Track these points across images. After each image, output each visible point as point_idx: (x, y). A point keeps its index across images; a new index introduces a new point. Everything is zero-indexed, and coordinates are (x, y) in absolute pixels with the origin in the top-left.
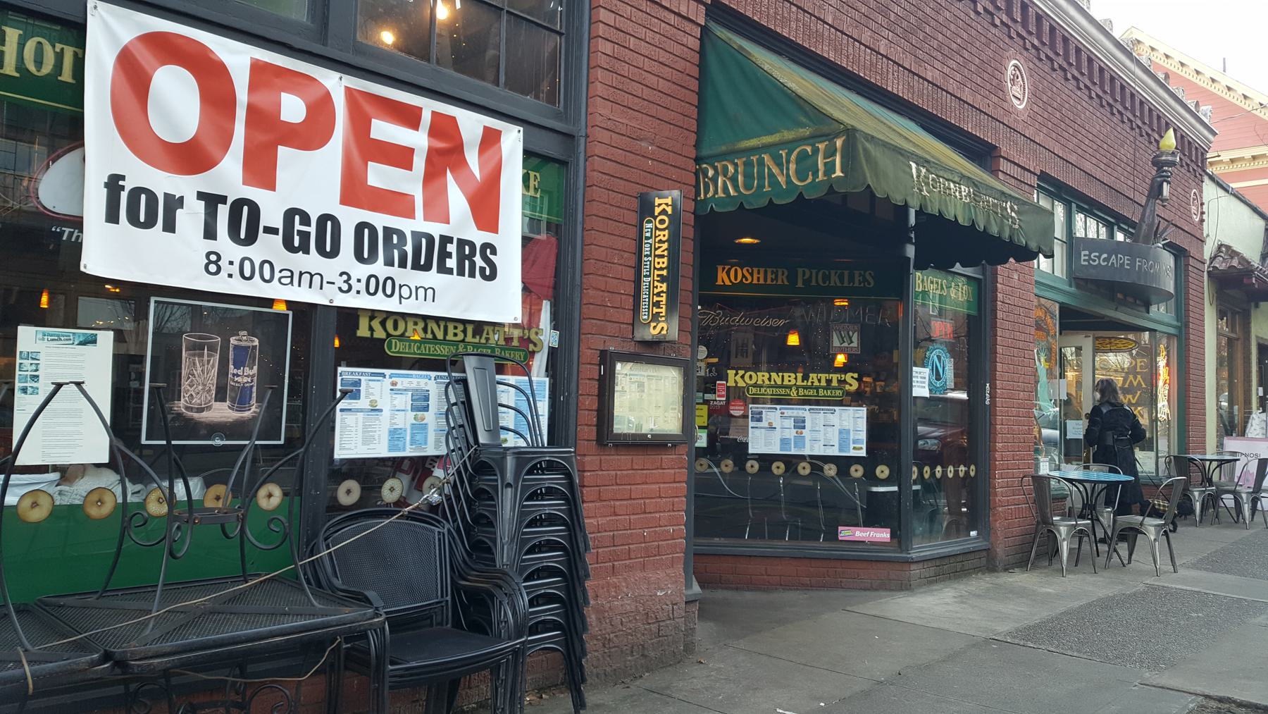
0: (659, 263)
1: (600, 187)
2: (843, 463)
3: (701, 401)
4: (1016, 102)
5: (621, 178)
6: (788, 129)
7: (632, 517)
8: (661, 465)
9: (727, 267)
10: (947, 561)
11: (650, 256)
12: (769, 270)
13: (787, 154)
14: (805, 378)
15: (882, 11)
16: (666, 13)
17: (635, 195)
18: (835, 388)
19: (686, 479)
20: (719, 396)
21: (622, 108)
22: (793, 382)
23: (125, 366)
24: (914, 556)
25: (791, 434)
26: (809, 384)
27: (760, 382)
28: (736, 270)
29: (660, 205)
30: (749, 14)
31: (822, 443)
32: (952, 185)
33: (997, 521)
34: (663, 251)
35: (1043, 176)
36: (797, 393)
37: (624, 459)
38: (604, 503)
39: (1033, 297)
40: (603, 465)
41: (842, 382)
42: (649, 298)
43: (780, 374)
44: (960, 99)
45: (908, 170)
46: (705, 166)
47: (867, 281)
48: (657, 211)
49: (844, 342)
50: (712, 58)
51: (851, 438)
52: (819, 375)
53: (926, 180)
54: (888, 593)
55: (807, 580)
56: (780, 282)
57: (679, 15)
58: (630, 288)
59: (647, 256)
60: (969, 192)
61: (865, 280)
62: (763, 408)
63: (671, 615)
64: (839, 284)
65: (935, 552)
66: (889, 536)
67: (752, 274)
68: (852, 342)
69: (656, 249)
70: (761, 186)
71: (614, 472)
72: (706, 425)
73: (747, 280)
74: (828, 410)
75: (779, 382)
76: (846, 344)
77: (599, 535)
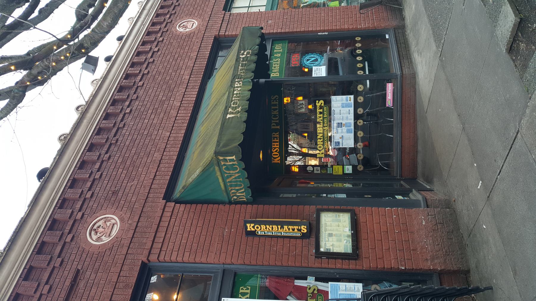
0: (275, 229)
1: (244, 258)
2: (357, 105)
3: (331, 168)
4: (194, 26)
5: (240, 246)
6: (216, 174)
7: (390, 239)
8: (365, 223)
9: (273, 159)
10: (401, 53)
11: (272, 232)
12: (273, 141)
13: (226, 174)
14: (319, 123)
15: (162, 104)
16: (171, 223)
17: (246, 238)
18: (323, 110)
19: (370, 208)
20: (329, 161)
21: (211, 246)
22: (321, 129)
23: (289, 64)
24: (399, 73)
25: (344, 129)
26: (322, 121)
27: (322, 143)
28: (273, 155)
29: (250, 228)
30: (168, 177)
31: (348, 115)
32: (235, 92)
33: (381, 26)
34: (270, 227)
35: (225, 9)
36: (326, 126)
37: (364, 244)
38: (384, 255)
39: (278, 11)
40: (367, 256)
41: (321, 107)
42: (291, 233)
43: (318, 134)
44: (196, 59)
45: (230, 119)
46: (232, 199)
47: (275, 98)
48: (253, 229)
49: (303, 107)
50: (189, 198)
51: (345, 102)
52: (318, 117)
53: (234, 109)
54: (417, 84)
55: (412, 121)
56: (278, 136)
57: (171, 216)
58: (287, 241)
59: (272, 233)
60: (237, 81)
61: (275, 99)
62: (333, 141)
63: (434, 216)
64: (278, 110)
65: (397, 60)
66: (390, 84)
67: (275, 148)
68: (302, 104)
69: (269, 230)
70: (240, 181)
71: (370, 250)
72: (342, 166)
73: (277, 150)
74: (333, 113)
75: (321, 135)
76: (304, 106)
77: (399, 258)
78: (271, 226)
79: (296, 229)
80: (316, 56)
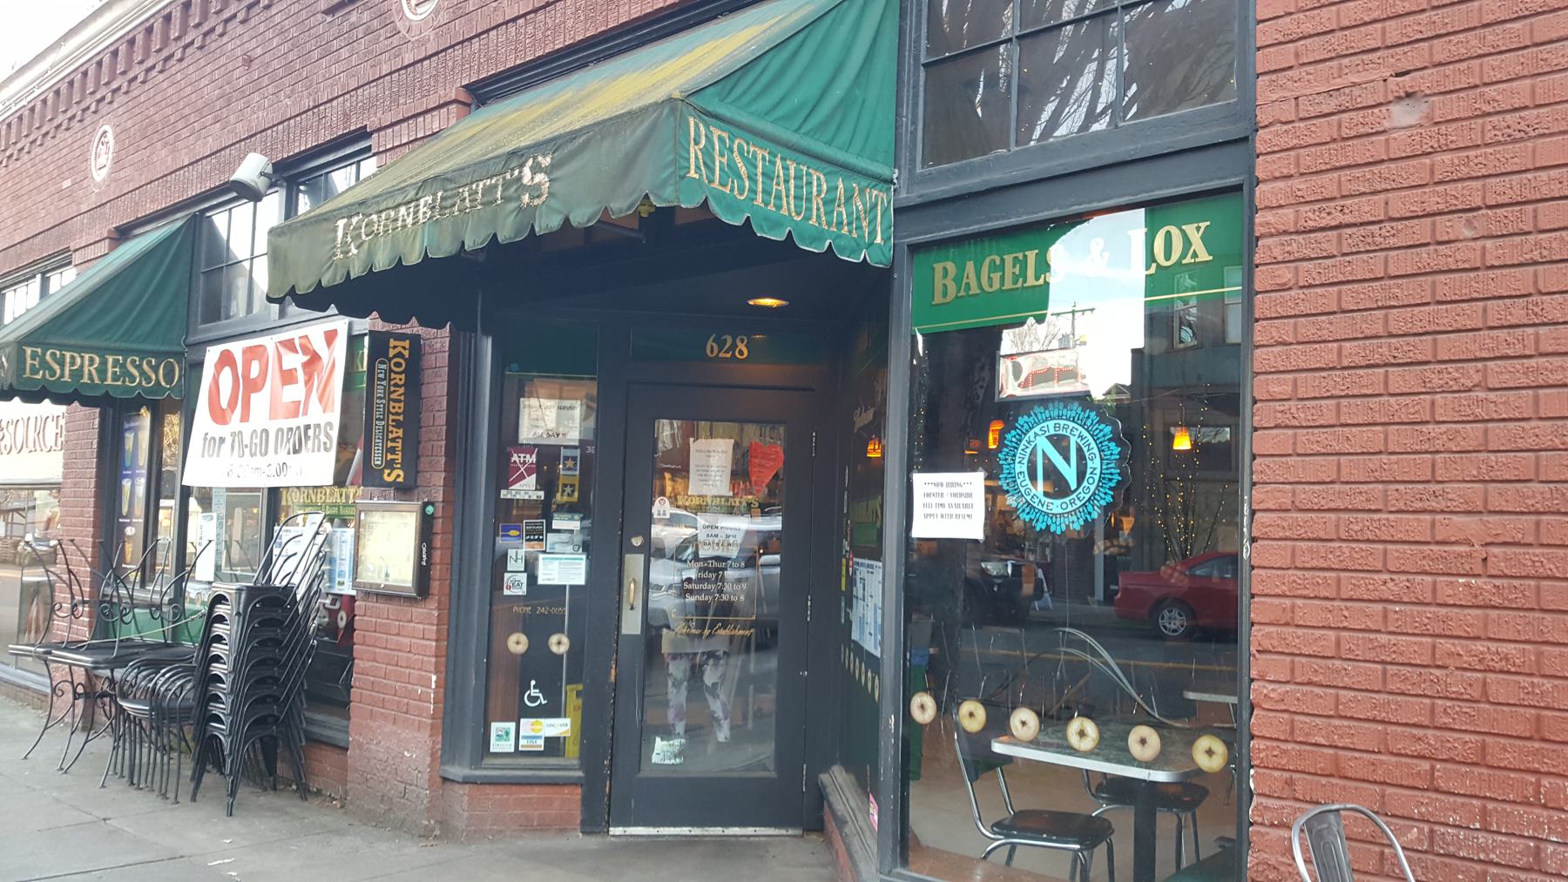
48: (392, 353)
78: (402, 398)
79: (394, 457)
80: (1090, 484)
